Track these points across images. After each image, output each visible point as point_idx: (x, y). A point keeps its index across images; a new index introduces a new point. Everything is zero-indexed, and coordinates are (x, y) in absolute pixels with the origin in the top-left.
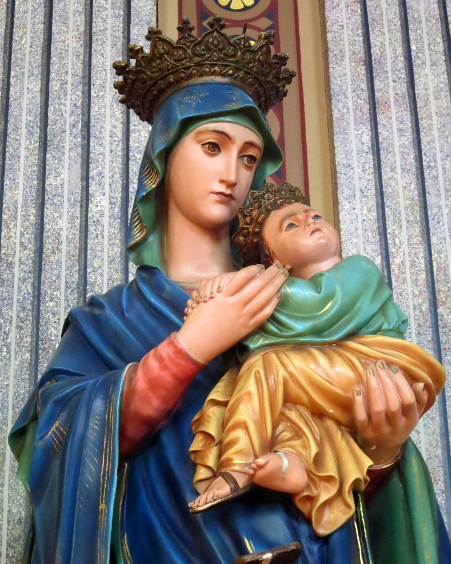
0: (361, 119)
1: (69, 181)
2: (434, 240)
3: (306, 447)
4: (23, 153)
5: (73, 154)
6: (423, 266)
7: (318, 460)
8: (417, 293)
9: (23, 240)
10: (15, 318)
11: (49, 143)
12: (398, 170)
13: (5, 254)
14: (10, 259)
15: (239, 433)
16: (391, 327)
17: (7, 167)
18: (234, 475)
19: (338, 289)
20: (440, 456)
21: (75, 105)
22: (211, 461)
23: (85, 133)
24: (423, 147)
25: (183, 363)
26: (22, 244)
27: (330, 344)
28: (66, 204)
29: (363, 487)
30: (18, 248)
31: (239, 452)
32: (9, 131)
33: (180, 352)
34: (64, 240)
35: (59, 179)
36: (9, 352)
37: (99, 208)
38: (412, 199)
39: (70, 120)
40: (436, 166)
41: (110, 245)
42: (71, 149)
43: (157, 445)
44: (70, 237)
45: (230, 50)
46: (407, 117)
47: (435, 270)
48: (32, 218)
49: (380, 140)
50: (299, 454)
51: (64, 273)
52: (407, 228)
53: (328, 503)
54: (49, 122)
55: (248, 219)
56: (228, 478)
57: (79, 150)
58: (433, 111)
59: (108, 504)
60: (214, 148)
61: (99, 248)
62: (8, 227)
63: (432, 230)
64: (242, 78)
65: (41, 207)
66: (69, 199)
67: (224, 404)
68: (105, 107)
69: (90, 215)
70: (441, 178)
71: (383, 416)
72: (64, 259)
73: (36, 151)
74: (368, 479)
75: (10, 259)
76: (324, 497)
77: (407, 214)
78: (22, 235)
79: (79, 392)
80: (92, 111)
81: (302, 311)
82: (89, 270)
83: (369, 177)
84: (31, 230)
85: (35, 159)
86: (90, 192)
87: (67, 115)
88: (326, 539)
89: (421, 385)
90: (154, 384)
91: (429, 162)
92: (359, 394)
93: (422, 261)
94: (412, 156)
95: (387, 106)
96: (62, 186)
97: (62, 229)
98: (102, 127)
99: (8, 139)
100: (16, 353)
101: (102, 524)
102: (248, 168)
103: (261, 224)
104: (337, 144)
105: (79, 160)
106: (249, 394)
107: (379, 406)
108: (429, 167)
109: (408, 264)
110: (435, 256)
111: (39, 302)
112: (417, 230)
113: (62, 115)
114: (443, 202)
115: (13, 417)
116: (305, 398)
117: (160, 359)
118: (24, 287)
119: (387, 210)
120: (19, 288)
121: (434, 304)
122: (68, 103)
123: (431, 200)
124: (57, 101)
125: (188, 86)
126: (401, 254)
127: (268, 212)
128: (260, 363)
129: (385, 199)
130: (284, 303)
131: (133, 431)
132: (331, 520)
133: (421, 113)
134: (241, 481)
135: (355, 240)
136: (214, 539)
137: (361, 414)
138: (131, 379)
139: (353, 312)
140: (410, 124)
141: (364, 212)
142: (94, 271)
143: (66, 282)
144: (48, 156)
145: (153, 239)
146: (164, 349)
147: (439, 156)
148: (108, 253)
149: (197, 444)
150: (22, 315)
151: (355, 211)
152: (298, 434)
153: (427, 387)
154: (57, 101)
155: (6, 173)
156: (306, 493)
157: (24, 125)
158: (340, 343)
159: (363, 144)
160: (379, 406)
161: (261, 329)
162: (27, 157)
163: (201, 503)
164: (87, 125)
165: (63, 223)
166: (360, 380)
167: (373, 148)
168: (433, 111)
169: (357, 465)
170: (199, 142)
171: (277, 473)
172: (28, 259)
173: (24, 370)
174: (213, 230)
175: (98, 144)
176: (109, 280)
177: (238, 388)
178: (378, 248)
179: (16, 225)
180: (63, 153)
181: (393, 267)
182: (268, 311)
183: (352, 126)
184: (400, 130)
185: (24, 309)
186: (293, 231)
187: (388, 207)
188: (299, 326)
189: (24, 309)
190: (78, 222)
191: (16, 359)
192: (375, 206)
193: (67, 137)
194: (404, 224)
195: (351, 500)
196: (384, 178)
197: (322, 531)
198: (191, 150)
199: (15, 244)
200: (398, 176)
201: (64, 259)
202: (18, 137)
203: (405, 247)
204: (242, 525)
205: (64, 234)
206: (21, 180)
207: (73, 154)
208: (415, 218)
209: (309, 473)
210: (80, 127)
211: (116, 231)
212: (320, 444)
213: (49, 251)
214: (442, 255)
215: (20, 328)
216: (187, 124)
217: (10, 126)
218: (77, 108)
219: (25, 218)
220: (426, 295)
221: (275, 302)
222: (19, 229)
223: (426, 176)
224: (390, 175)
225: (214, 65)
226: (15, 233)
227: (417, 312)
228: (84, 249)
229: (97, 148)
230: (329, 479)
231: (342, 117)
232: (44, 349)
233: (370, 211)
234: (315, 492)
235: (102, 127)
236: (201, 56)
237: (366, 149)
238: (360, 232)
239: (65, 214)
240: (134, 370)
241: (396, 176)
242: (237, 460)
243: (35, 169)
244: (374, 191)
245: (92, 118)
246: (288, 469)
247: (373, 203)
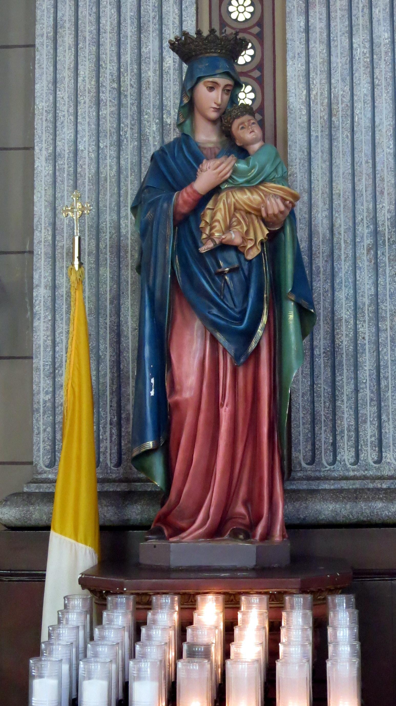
0: (301, 12)
1: (153, 50)
2: (333, 81)
3: (242, 228)
4: (129, 34)
5: (154, 34)
6: (326, 96)
7: (247, 232)
8: (322, 110)
9: (132, 83)
10: (129, 124)
11: (142, 28)
12: (318, 42)
13: (123, 90)
14: (126, 93)
15: (216, 224)
16: (279, 176)
17: (122, 42)
18: (215, 239)
19: (257, 163)
20: (328, 192)
21: (154, 6)
22: (207, 232)
23: (160, 22)
24: (331, 29)
25: (196, 195)
26: (131, 85)
27: (253, 186)
28: (152, 63)
29: (265, 241)
30: (129, 87)
31: (216, 231)
32: (121, 22)
33: (195, 191)
34: (151, 83)
35: (148, 48)
36: (127, 142)
37: (168, 65)
38: (324, 59)
39: (152, 14)
40: (337, 40)
41: (174, 85)
42: (153, 31)
43: (188, 223)
44: (154, 80)
45: (218, 42)
46: (324, 10)
47: (332, 97)
48: (135, 70)
49: (310, 25)
50: (239, 231)
51: (152, 100)
52: (320, 74)
53: (251, 248)
54: (142, 16)
55: (226, 121)
56: (213, 241)
57: (157, 32)
58: (338, 8)
59: (169, 247)
60: (211, 89)
61: (168, 87)
62: (124, 76)
63: (332, 76)
64: (224, 53)
65: (140, 65)
66: (153, 60)
67: (213, 209)
68: (170, 7)
69: (164, 68)
70: (339, 46)
71: (273, 215)
72: (151, 93)
73: (136, 33)
74: (267, 238)
75: (126, 93)
76: (249, 246)
77: (320, 67)
78: (131, 80)
79: (159, 199)
80: (163, 9)
81: (242, 174)
82: (164, 99)
83: (302, 46)
84: (135, 77)
85: (135, 38)
86: (163, 55)
87: (150, 12)
88: (250, 261)
89: (288, 202)
90: (185, 202)
91: (334, 37)
92: (263, 207)
93: (326, 93)
94: (325, 34)
95: (314, 4)
96: (149, 52)
97: (150, 76)
98: (168, 19)
99: (121, 26)
100: (131, 142)
101: (168, 255)
102: (227, 94)
103: (231, 124)
104: (287, 27)
105: (157, 38)
106: (221, 209)
107: (270, 212)
108: (333, 40)
109: (319, 94)
110: (333, 90)
111: (140, 115)
112: (325, 75)
113: (148, 12)
114: (339, 60)
115: (132, 198)
116: (242, 208)
117: (188, 194)
118: (133, 108)
119: (311, 64)
120: (131, 109)
121: (330, 115)
122: (151, 4)
123: (333, 59)
124: (145, 4)
125: (201, 58)
126: (316, 89)
127: (234, 119)
128: (225, 196)
129: (310, 58)
130: (235, 171)
131: (178, 218)
132: (252, 255)
133: (332, 8)
134: (217, 242)
135: (294, 82)
136: (209, 261)
137: (264, 214)
138: (177, 199)
139: (263, 172)
140: (325, 15)
141: (299, 66)
142: (167, 99)
143: (153, 105)
144: (142, 36)
145: (188, 122)
146: (189, 189)
147: (339, 34)
148: (173, 89)
149: (202, 225)
150: (133, 122)
151: (295, 66)
152: (239, 223)
153: (291, 202)
154: (145, 4)
155: (121, 45)
156: (242, 245)
157: (129, 18)
158: (256, 186)
159: (300, 27)
160: (270, 212)
161: (226, 181)
162: (131, 37)
163: (203, 249)
164: (161, 18)
165: (151, 73)
166: (263, 201)
167: (305, 30)
168: (338, 8)
169: (262, 233)
170: (205, 86)
171: (231, 240)
172: (134, 93)
173: (135, 150)
174: (213, 122)
175: (167, 29)
176: (174, 103)
177: (217, 205)
178: (305, 86)
179: (127, 74)
180: (149, 34)
181: (312, 96)
182: (228, 175)
183: (296, 16)
184: (320, 19)
185: (133, 119)
186: (243, 131)
187: (311, 63)
188: (241, 180)
189: (133, 119)
190: (158, 72)
191: (131, 145)
192: (304, 63)
193: (151, 25)
194: (319, 72)
195: (259, 247)
196: (310, 46)
197: (249, 257)
198: (202, 89)
199: (127, 85)
200: (317, 45)
201: (151, 93)
202: (126, 25)
203: (318, 85)
204: (219, 256)
205: (151, 79)
206: (129, 50)
207: (154, 34)
208: (324, 69)
209: (243, 238)
210: (157, 19)
211: (177, 77)
212: (248, 226)
213: (144, 88)
214: (337, 90)
215: (132, 129)
216: (199, 79)
217: (122, 19)
218: (155, 7)
219: (132, 70)
220: (327, 111)
221: (231, 171)
222: (129, 77)
223: (332, 46)
224: (313, 45)
225: (211, 49)
226: (127, 79)
227: (322, 120)
228: (161, 87)
229: (166, 31)
230: (251, 240)
231: (291, 12)
232: (144, 140)
233: (302, 65)
234: (246, 244)
235: (168, 19)
236: (206, 45)
237: (302, 30)
238: (296, 77)
239: (151, 68)
240: (178, 196)
241: (316, 46)
242: (217, 234)
243: (136, 43)
244: (304, 54)
245: (163, 13)
246: (235, 237)
247: (303, 60)
